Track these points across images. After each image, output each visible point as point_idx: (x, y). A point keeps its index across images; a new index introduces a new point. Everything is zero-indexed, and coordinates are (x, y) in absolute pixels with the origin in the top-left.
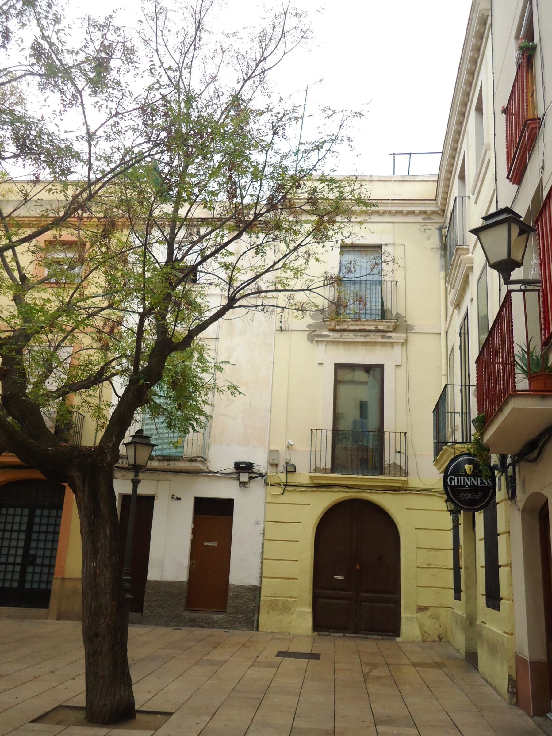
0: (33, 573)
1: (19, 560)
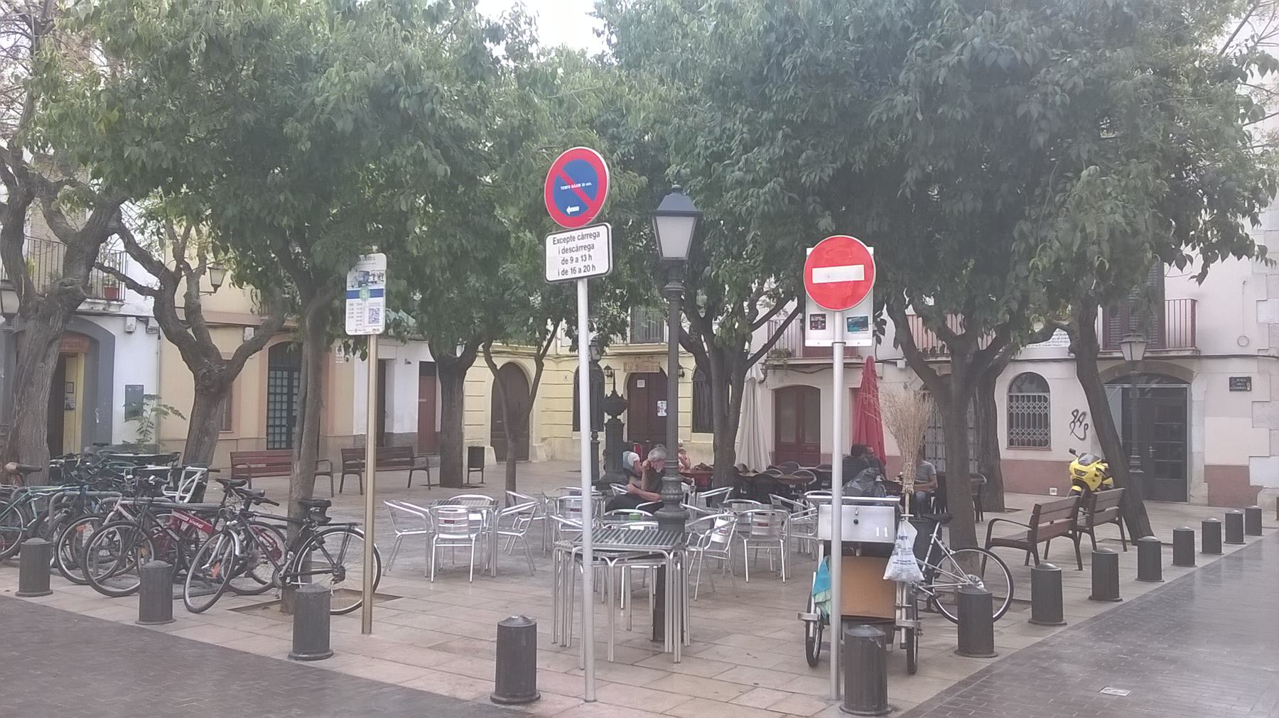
1: (284, 422)
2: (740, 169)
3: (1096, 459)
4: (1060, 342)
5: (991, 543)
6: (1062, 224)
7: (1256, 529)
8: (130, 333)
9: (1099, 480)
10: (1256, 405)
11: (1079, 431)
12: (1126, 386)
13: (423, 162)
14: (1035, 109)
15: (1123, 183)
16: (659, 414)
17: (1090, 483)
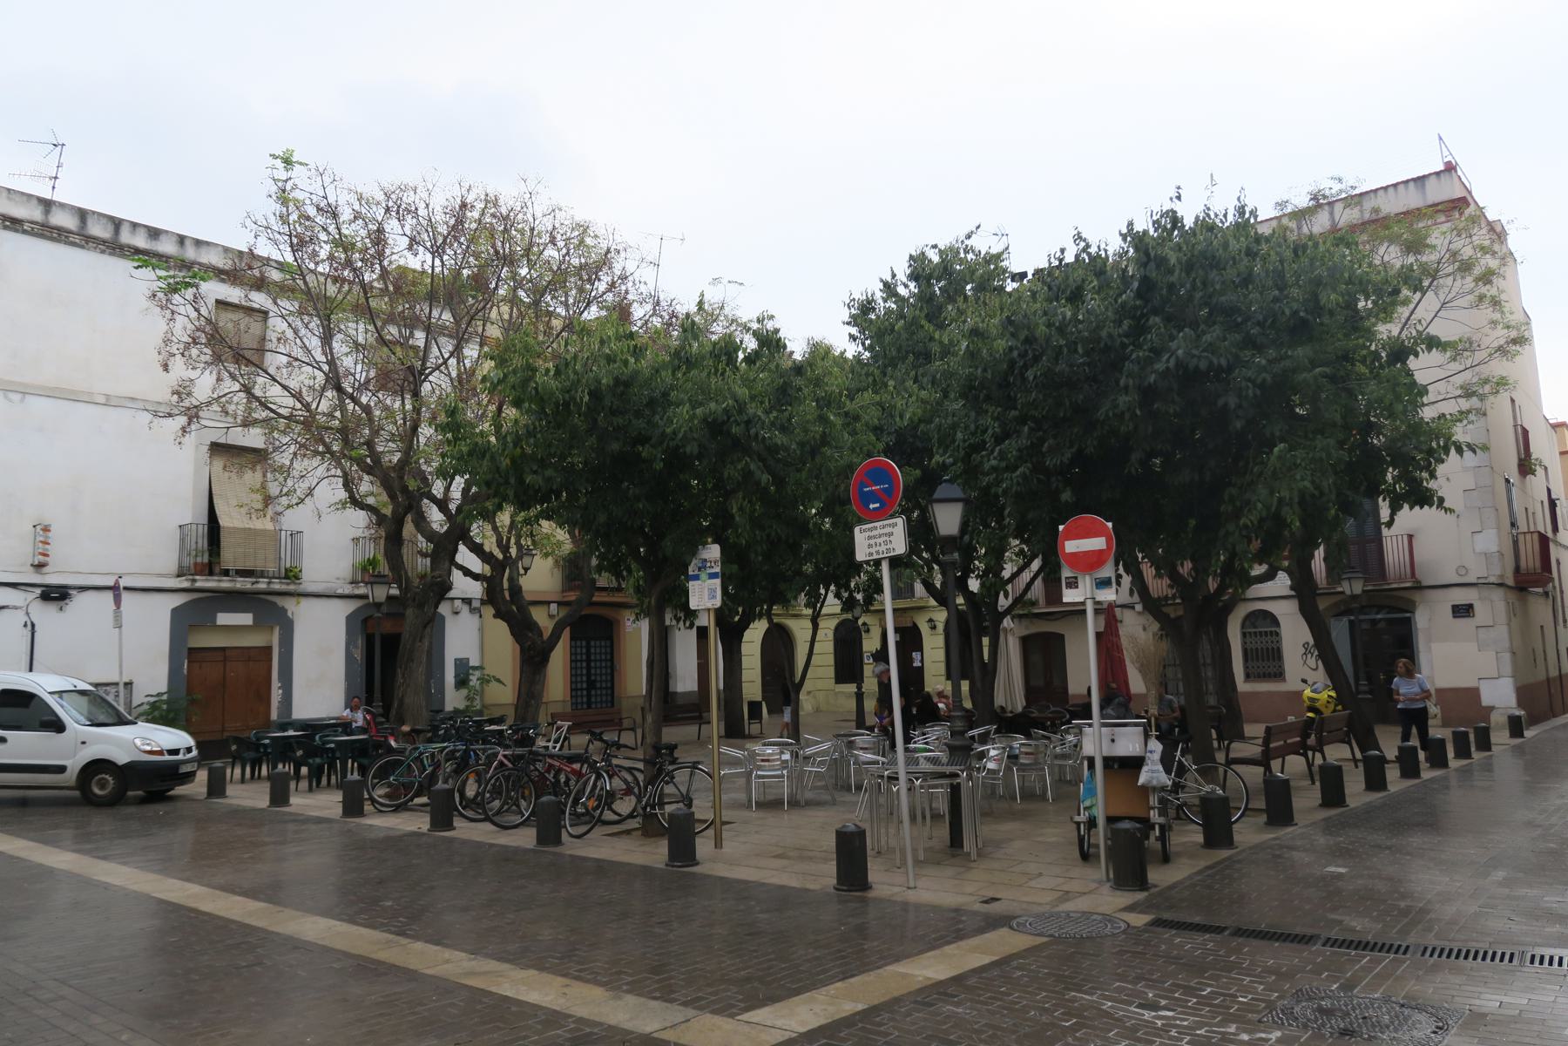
0: (596, 695)
1: (585, 686)
2: (995, 458)
3: (1326, 686)
4: (1282, 583)
5: (1230, 762)
6: (1262, 491)
7: (1485, 743)
8: (457, 613)
9: (1332, 707)
10: (1480, 629)
11: (1312, 662)
12: (1352, 618)
13: (750, 473)
14: (1232, 401)
15: (1310, 456)
16: (915, 665)
17: (1323, 709)
